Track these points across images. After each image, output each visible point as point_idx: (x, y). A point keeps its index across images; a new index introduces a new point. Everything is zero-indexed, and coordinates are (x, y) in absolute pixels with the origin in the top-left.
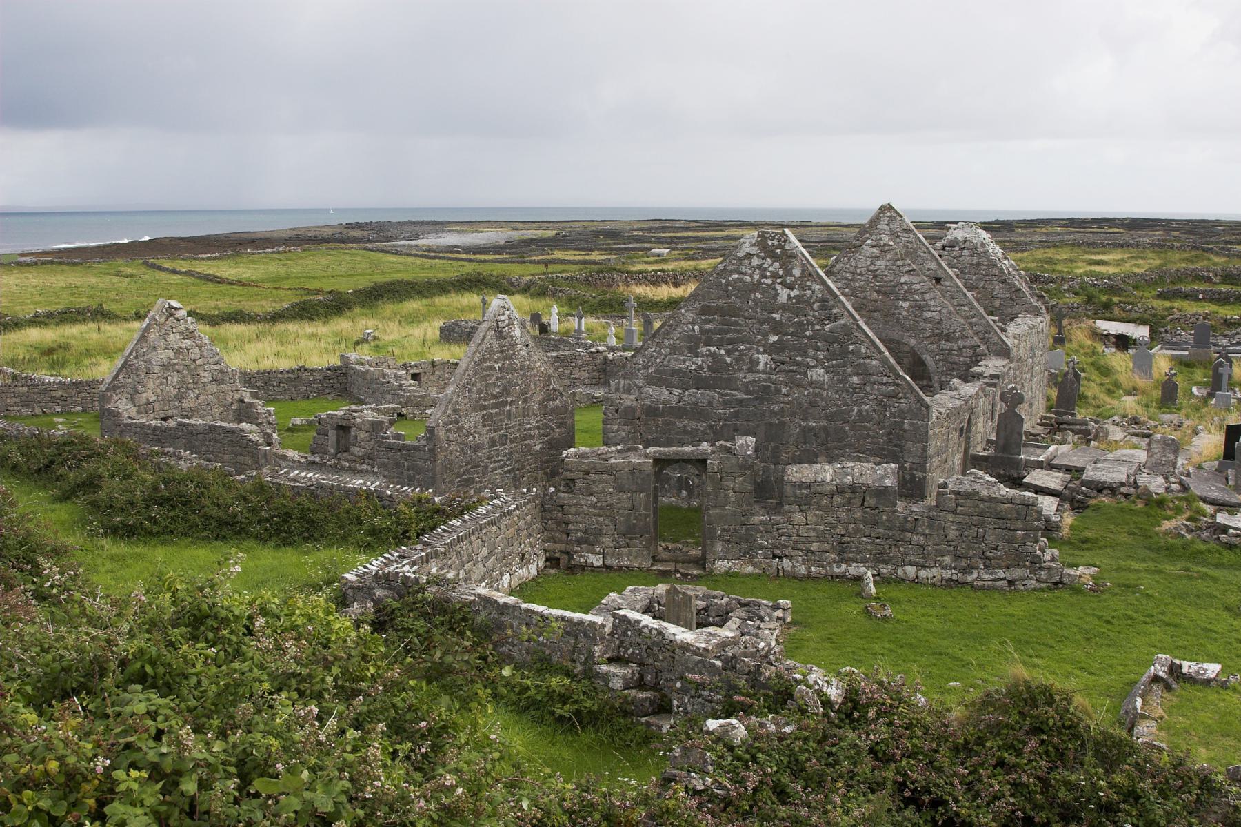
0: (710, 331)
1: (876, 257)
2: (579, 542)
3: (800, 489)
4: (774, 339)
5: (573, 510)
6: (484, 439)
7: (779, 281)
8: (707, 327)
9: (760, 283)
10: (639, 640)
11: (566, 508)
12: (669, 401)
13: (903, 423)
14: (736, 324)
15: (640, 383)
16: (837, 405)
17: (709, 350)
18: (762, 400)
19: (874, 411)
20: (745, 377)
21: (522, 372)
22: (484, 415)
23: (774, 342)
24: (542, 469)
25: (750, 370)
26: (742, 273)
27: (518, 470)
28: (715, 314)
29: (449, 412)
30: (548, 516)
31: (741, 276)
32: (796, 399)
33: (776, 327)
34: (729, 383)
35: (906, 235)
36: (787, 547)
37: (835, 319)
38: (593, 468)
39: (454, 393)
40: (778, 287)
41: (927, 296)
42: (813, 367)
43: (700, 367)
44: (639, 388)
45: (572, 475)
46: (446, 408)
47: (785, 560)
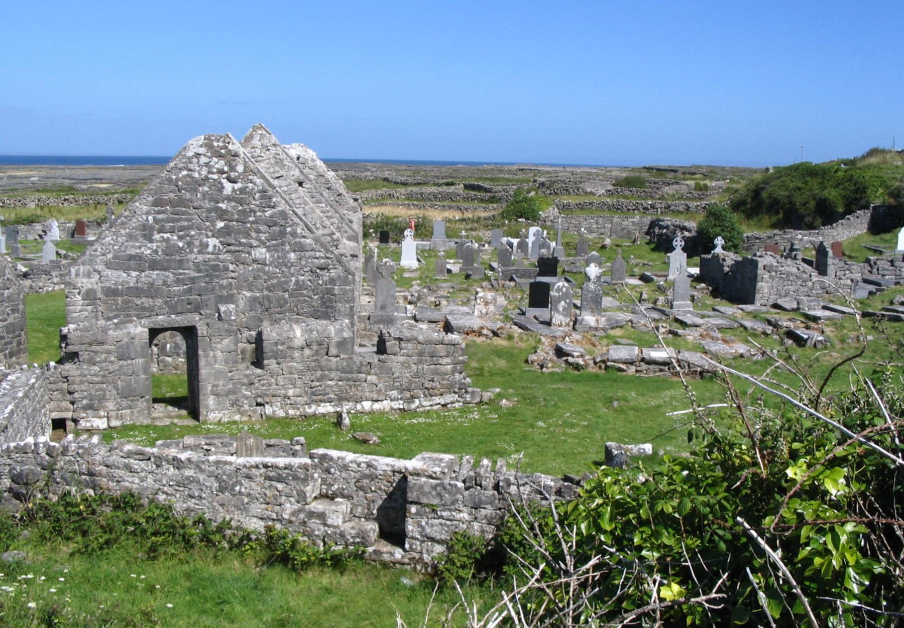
4: (220, 224)
7: (224, 176)
8: (160, 216)
16: (278, 277)
17: (163, 237)
20: (196, 258)
23: (221, 228)
25: (200, 252)
28: (167, 205)
30: (53, 386)
31: (190, 173)
33: (222, 215)
35: (274, 148)
40: (224, 181)
42: (256, 247)
43: (156, 252)
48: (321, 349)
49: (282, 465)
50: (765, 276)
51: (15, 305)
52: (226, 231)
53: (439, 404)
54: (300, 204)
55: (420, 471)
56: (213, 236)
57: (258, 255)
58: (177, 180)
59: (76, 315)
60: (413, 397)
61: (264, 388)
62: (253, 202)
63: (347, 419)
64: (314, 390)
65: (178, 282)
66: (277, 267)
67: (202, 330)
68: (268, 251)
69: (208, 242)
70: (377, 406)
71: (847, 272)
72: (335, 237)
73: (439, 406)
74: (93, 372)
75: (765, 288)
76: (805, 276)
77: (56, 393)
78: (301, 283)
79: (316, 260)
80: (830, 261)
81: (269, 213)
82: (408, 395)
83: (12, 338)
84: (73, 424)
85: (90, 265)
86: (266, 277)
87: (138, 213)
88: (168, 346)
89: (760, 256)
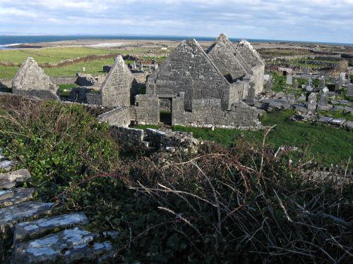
34: (178, 79)
52: (192, 69)
65: (177, 84)
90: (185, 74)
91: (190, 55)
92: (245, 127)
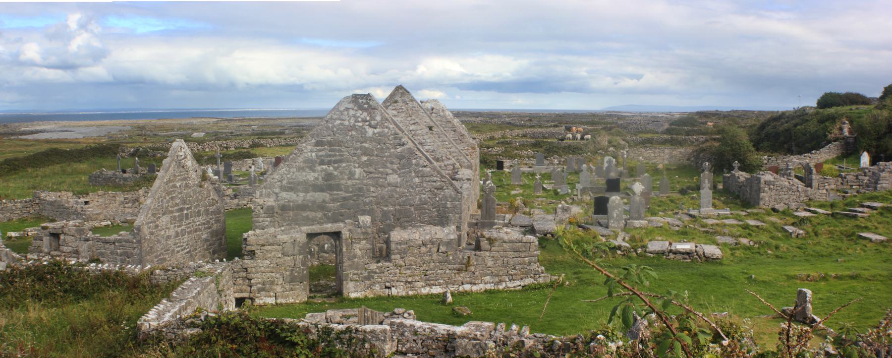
0: (322, 156)
1: (395, 116)
2: (259, 290)
3: (400, 245)
4: (365, 158)
5: (254, 270)
6: (172, 232)
7: (367, 123)
8: (320, 153)
9: (354, 125)
10: (415, 338)
11: (249, 270)
12: (297, 201)
13: (447, 204)
14: (340, 151)
15: (277, 190)
16: (406, 196)
17: (322, 168)
18: (358, 196)
19: (429, 198)
20: (346, 183)
21: (193, 188)
22: (171, 217)
23: (365, 161)
24: (207, 250)
25: (349, 179)
26: (343, 120)
27: (193, 251)
28: (326, 145)
29: (150, 215)
30: (236, 275)
31: (342, 122)
32: (379, 194)
33: (366, 152)
34: (338, 187)
35: (412, 103)
36: (393, 281)
37: (403, 145)
38: (267, 242)
39: (152, 203)
40: (367, 127)
41: (425, 137)
42: (390, 174)
43: (317, 179)
44: (277, 194)
45: (253, 248)
46: (148, 214)
47: (393, 289)
48: (434, 247)
49: (368, 330)
50: (765, 189)
51: (218, 217)
52: (369, 163)
53: (520, 285)
54: (430, 142)
55: (465, 335)
56: (359, 167)
57: (391, 180)
58: (333, 127)
59: (260, 224)
60: (501, 281)
61: (391, 276)
62: (389, 142)
63: (450, 297)
64: (428, 277)
65: (333, 200)
66: (405, 188)
67: (346, 234)
68: (400, 177)
69: (355, 171)
70: (475, 288)
71: (826, 184)
72: (456, 166)
73: (519, 287)
74: (265, 265)
75: (767, 198)
76: (794, 187)
77: (238, 279)
78: (423, 200)
79: (434, 183)
80: (814, 177)
81: (399, 149)
82: (497, 279)
83: (215, 240)
84: (250, 301)
85: (270, 189)
86: (398, 196)
87: (305, 151)
88: (326, 246)
89: (763, 175)
90: (351, 175)
91: (363, 132)
92: (518, 283)
